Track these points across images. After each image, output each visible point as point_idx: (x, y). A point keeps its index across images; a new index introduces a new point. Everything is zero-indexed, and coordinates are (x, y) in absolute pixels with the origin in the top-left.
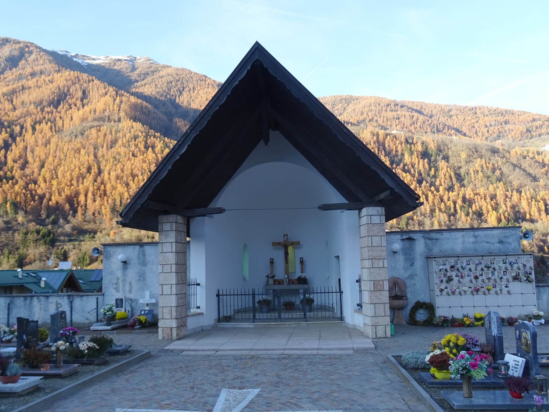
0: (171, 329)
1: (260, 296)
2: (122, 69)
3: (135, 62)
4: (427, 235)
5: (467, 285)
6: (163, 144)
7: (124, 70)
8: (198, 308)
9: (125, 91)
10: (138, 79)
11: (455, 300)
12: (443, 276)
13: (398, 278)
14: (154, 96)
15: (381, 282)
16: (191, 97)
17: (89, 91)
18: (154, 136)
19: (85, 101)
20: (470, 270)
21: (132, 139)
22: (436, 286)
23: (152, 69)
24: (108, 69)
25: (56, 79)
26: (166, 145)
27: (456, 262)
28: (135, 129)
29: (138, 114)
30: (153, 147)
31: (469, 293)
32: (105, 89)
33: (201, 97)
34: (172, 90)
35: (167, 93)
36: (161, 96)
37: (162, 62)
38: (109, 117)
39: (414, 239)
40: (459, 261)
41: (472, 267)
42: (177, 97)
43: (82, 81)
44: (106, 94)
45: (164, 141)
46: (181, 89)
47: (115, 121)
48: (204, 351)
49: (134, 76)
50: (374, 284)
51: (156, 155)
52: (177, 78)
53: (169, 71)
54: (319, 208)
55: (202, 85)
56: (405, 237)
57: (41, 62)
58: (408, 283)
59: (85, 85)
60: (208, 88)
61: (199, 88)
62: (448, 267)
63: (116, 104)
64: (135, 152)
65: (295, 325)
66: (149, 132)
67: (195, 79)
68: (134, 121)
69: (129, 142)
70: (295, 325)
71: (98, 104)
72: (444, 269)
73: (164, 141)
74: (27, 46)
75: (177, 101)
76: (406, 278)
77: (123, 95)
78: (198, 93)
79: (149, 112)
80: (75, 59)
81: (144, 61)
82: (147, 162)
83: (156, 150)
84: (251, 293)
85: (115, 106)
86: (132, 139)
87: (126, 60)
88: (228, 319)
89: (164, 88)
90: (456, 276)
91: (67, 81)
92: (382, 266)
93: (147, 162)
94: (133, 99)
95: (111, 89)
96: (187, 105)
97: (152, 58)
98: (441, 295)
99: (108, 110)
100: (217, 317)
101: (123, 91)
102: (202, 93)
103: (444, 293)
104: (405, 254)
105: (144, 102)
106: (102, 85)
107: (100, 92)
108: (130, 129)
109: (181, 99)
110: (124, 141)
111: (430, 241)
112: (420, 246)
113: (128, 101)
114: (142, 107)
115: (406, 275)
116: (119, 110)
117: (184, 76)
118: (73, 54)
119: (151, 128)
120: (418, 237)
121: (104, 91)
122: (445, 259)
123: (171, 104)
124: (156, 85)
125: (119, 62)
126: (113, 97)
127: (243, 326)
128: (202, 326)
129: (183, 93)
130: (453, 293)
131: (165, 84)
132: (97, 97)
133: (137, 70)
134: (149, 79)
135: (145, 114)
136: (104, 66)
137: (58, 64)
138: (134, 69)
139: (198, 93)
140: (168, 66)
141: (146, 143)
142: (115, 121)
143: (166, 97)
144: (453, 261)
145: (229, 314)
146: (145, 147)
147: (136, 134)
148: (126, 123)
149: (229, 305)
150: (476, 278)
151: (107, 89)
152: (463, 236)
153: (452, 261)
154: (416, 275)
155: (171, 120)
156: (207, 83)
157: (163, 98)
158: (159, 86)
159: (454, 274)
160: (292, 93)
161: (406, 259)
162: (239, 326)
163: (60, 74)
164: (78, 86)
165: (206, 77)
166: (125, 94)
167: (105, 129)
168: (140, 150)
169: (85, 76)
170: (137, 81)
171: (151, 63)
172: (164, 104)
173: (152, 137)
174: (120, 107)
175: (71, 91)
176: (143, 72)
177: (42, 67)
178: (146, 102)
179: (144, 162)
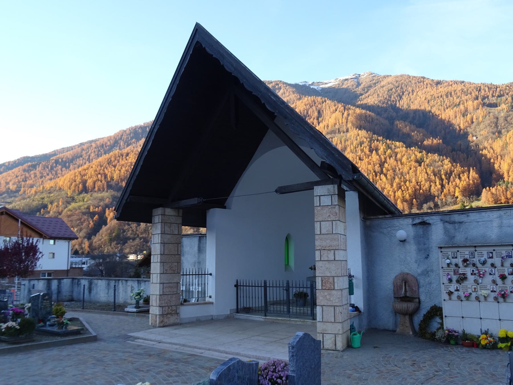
0: (156, 315)
1: (298, 289)
2: (348, 87)
3: (360, 78)
4: (447, 218)
5: (488, 287)
6: (385, 146)
7: (350, 87)
8: (210, 297)
9: (351, 105)
10: (362, 92)
11: (470, 308)
12: (452, 273)
13: (407, 274)
14: (376, 104)
15: (331, 280)
16: (410, 100)
17: (323, 111)
18: (378, 140)
19: (320, 119)
20: (493, 265)
21: (358, 145)
22: (443, 286)
23: (374, 81)
24: (337, 89)
25: (298, 105)
26: (388, 146)
27: (472, 255)
28: (360, 136)
29: (363, 123)
30: (377, 150)
31: (491, 299)
32: (335, 106)
33: (420, 98)
34: (392, 97)
35: (388, 100)
36: (383, 103)
37: (382, 74)
38: (339, 129)
39: (429, 224)
40: (476, 253)
41: (497, 261)
42: (398, 102)
43: (317, 104)
44: (336, 110)
45: (386, 143)
46: (401, 94)
47: (344, 132)
48: (152, 341)
49: (359, 90)
50: (322, 281)
51: (380, 156)
52: (397, 85)
53: (389, 80)
54: (276, 191)
55: (420, 86)
56: (417, 221)
57: (287, 94)
58: (422, 281)
59: (319, 106)
60: (427, 88)
61: (418, 90)
62: (459, 261)
63: (344, 117)
64: (362, 156)
65: (300, 323)
66: (372, 137)
67: (413, 82)
68: (360, 129)
69: (356, 148)
70: (300, 323)
71: (330, 120)
72: (454, 263)
73: (386, 143)
74: (277, 84)
75: (397, 105)
76: (419, 275)
77: (350, 109)
78: (417, 95)
79: (372, 119)
80: (312, 87)
81: (367, 76)
82: (372, 163)
83: (380, 152)
84: (263, 285)
85: (344, 119)
86: (358, 145)
87: (351, 79)
88: (248, 310)
89: (385, 96)
90: (472, 274)
91: (306, 105)
92: (333, 258)
93: (372, 163)
94: (358, 111)
95: (340, 106)
96: (407, 107)
97: (373, 71)
98: (450, 299)
99: (338, 124)
100: (235, 307)
101: (349, 106)
102: (421, 93)
103: (454, 297)
104: (418, 243)
105: (368, 112)
106: (333, 104)
107: (332, 110)
108: (356, 137)
109: (401, 103)
110: (352, 148)
111: (452, 225)
112: (437, 232)
113: (354, 113)
114: (366, 116)
115: (419, 271)
116: (347, 122)
117: (403, 81)
118: (310, 83)
119: (374, 134)
120: (433, 220)
121: (334, 108)
122: (455, 250)
123: (392, 109)
124: (378, 95)
125: (346, 81)
126: (342, 112)
127: (255, 319)
128: (212, 316)
129: (403, 97)
130: (468, 297)
131: (386, 92)
132: (329, 114)
133: (362, 85)
134: (372, 90)
135: (369, 122)
136: (334, 88)
137: (299, 93)
138: (359, 84)
139: (417, 95)
140: (388, 76)
141: (370, 147)
142: (344, 132)
143: (387, 103)
144: (467, 253)
145: (248, 306)
146: (370, 151)
147: (362, 140)
148: (353, 132)
149: (242, 297)
150: (503, 277)
151: (336, 106)
152: (500, 217)
153: (466, 253)
154: (432, 271)
155: (392, 123)
156: (425, 83)
157: (385, 105)
158: (381, 95)
159: (468, 271)
160: (225, 67)
161: (419, 250)
162: (251, 318)
163: (301, 101)
164: (314, 108)
165: (424, 78)
166: (352, 107)
167: (336, 140)
168: (365, 154)
169: (319, 99)
170: (362, 95)
171: (373, 77)
172: (385, 110)
173: (375, 142)
174: (347, 119)
175: (309, 113)
176: (366, 86)
177: (288, 98)
178: (370, 111)
179: (369, 163)
